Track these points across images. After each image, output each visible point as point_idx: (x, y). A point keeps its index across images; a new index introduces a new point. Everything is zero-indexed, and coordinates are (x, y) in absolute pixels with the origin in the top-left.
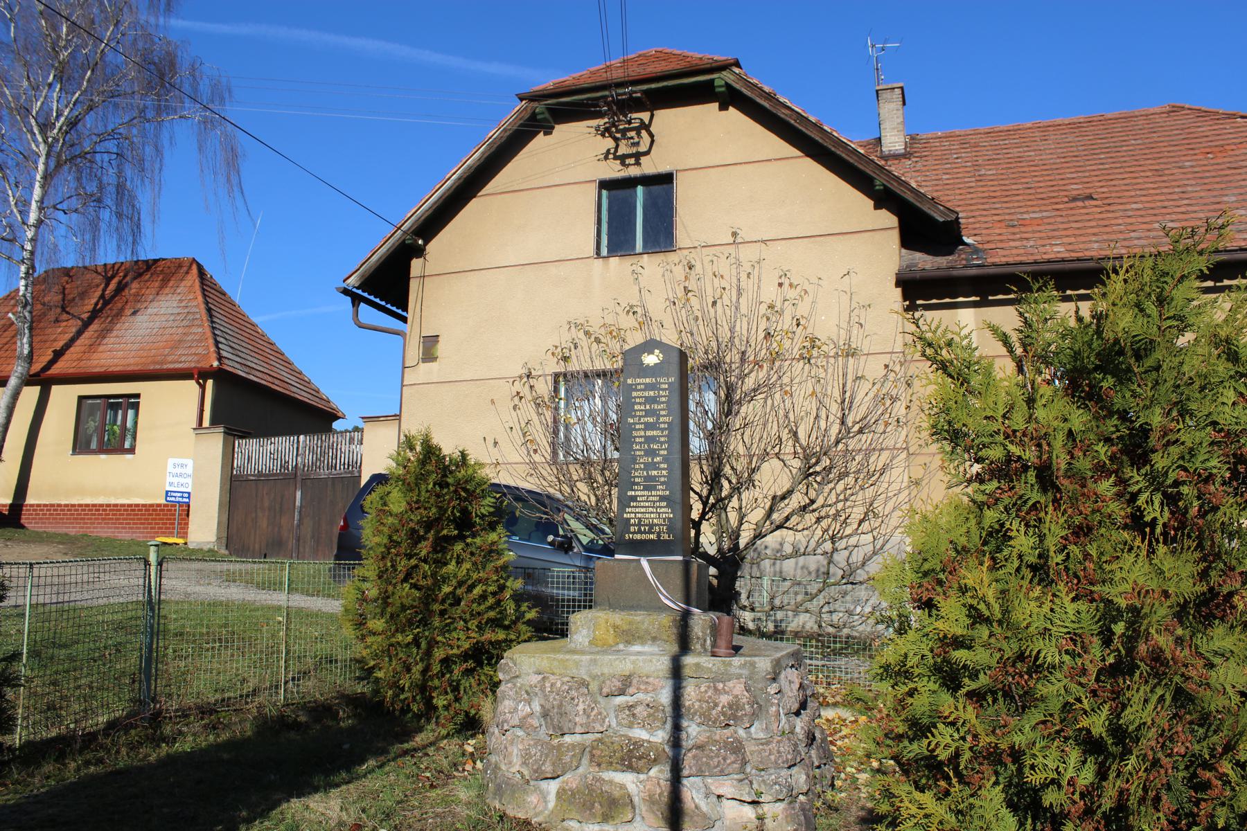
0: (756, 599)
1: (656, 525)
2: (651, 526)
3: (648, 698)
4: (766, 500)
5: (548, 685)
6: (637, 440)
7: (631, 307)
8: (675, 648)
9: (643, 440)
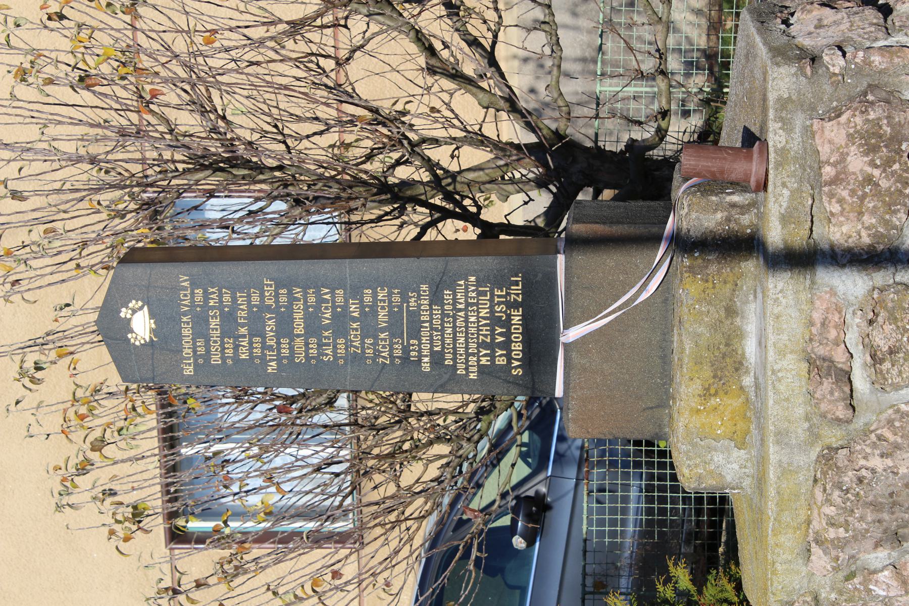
0: (639, 109)
1: (492, 311)
2: (494, 321)
3: (856, 322)
4: (435, 89)
5: (832, 533)
6: (313, 352)
7: (23, 373)
8: (751, 266)
9: (313, 340)
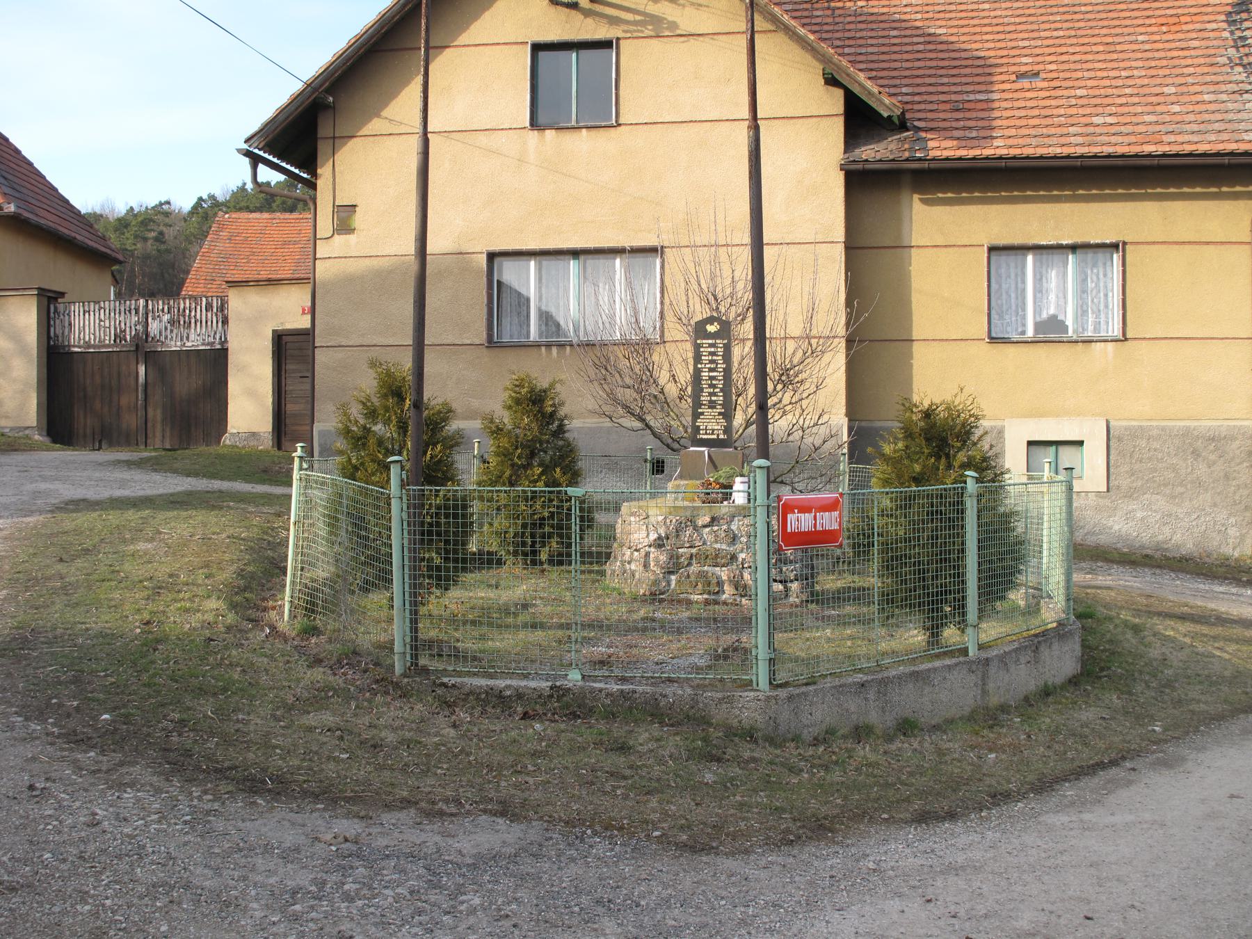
5: (668, 521)
